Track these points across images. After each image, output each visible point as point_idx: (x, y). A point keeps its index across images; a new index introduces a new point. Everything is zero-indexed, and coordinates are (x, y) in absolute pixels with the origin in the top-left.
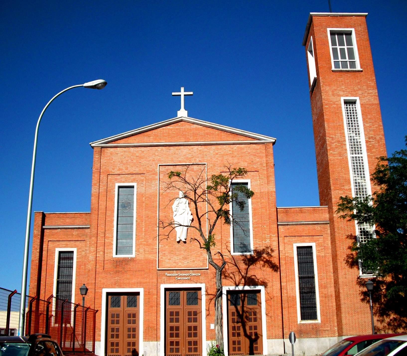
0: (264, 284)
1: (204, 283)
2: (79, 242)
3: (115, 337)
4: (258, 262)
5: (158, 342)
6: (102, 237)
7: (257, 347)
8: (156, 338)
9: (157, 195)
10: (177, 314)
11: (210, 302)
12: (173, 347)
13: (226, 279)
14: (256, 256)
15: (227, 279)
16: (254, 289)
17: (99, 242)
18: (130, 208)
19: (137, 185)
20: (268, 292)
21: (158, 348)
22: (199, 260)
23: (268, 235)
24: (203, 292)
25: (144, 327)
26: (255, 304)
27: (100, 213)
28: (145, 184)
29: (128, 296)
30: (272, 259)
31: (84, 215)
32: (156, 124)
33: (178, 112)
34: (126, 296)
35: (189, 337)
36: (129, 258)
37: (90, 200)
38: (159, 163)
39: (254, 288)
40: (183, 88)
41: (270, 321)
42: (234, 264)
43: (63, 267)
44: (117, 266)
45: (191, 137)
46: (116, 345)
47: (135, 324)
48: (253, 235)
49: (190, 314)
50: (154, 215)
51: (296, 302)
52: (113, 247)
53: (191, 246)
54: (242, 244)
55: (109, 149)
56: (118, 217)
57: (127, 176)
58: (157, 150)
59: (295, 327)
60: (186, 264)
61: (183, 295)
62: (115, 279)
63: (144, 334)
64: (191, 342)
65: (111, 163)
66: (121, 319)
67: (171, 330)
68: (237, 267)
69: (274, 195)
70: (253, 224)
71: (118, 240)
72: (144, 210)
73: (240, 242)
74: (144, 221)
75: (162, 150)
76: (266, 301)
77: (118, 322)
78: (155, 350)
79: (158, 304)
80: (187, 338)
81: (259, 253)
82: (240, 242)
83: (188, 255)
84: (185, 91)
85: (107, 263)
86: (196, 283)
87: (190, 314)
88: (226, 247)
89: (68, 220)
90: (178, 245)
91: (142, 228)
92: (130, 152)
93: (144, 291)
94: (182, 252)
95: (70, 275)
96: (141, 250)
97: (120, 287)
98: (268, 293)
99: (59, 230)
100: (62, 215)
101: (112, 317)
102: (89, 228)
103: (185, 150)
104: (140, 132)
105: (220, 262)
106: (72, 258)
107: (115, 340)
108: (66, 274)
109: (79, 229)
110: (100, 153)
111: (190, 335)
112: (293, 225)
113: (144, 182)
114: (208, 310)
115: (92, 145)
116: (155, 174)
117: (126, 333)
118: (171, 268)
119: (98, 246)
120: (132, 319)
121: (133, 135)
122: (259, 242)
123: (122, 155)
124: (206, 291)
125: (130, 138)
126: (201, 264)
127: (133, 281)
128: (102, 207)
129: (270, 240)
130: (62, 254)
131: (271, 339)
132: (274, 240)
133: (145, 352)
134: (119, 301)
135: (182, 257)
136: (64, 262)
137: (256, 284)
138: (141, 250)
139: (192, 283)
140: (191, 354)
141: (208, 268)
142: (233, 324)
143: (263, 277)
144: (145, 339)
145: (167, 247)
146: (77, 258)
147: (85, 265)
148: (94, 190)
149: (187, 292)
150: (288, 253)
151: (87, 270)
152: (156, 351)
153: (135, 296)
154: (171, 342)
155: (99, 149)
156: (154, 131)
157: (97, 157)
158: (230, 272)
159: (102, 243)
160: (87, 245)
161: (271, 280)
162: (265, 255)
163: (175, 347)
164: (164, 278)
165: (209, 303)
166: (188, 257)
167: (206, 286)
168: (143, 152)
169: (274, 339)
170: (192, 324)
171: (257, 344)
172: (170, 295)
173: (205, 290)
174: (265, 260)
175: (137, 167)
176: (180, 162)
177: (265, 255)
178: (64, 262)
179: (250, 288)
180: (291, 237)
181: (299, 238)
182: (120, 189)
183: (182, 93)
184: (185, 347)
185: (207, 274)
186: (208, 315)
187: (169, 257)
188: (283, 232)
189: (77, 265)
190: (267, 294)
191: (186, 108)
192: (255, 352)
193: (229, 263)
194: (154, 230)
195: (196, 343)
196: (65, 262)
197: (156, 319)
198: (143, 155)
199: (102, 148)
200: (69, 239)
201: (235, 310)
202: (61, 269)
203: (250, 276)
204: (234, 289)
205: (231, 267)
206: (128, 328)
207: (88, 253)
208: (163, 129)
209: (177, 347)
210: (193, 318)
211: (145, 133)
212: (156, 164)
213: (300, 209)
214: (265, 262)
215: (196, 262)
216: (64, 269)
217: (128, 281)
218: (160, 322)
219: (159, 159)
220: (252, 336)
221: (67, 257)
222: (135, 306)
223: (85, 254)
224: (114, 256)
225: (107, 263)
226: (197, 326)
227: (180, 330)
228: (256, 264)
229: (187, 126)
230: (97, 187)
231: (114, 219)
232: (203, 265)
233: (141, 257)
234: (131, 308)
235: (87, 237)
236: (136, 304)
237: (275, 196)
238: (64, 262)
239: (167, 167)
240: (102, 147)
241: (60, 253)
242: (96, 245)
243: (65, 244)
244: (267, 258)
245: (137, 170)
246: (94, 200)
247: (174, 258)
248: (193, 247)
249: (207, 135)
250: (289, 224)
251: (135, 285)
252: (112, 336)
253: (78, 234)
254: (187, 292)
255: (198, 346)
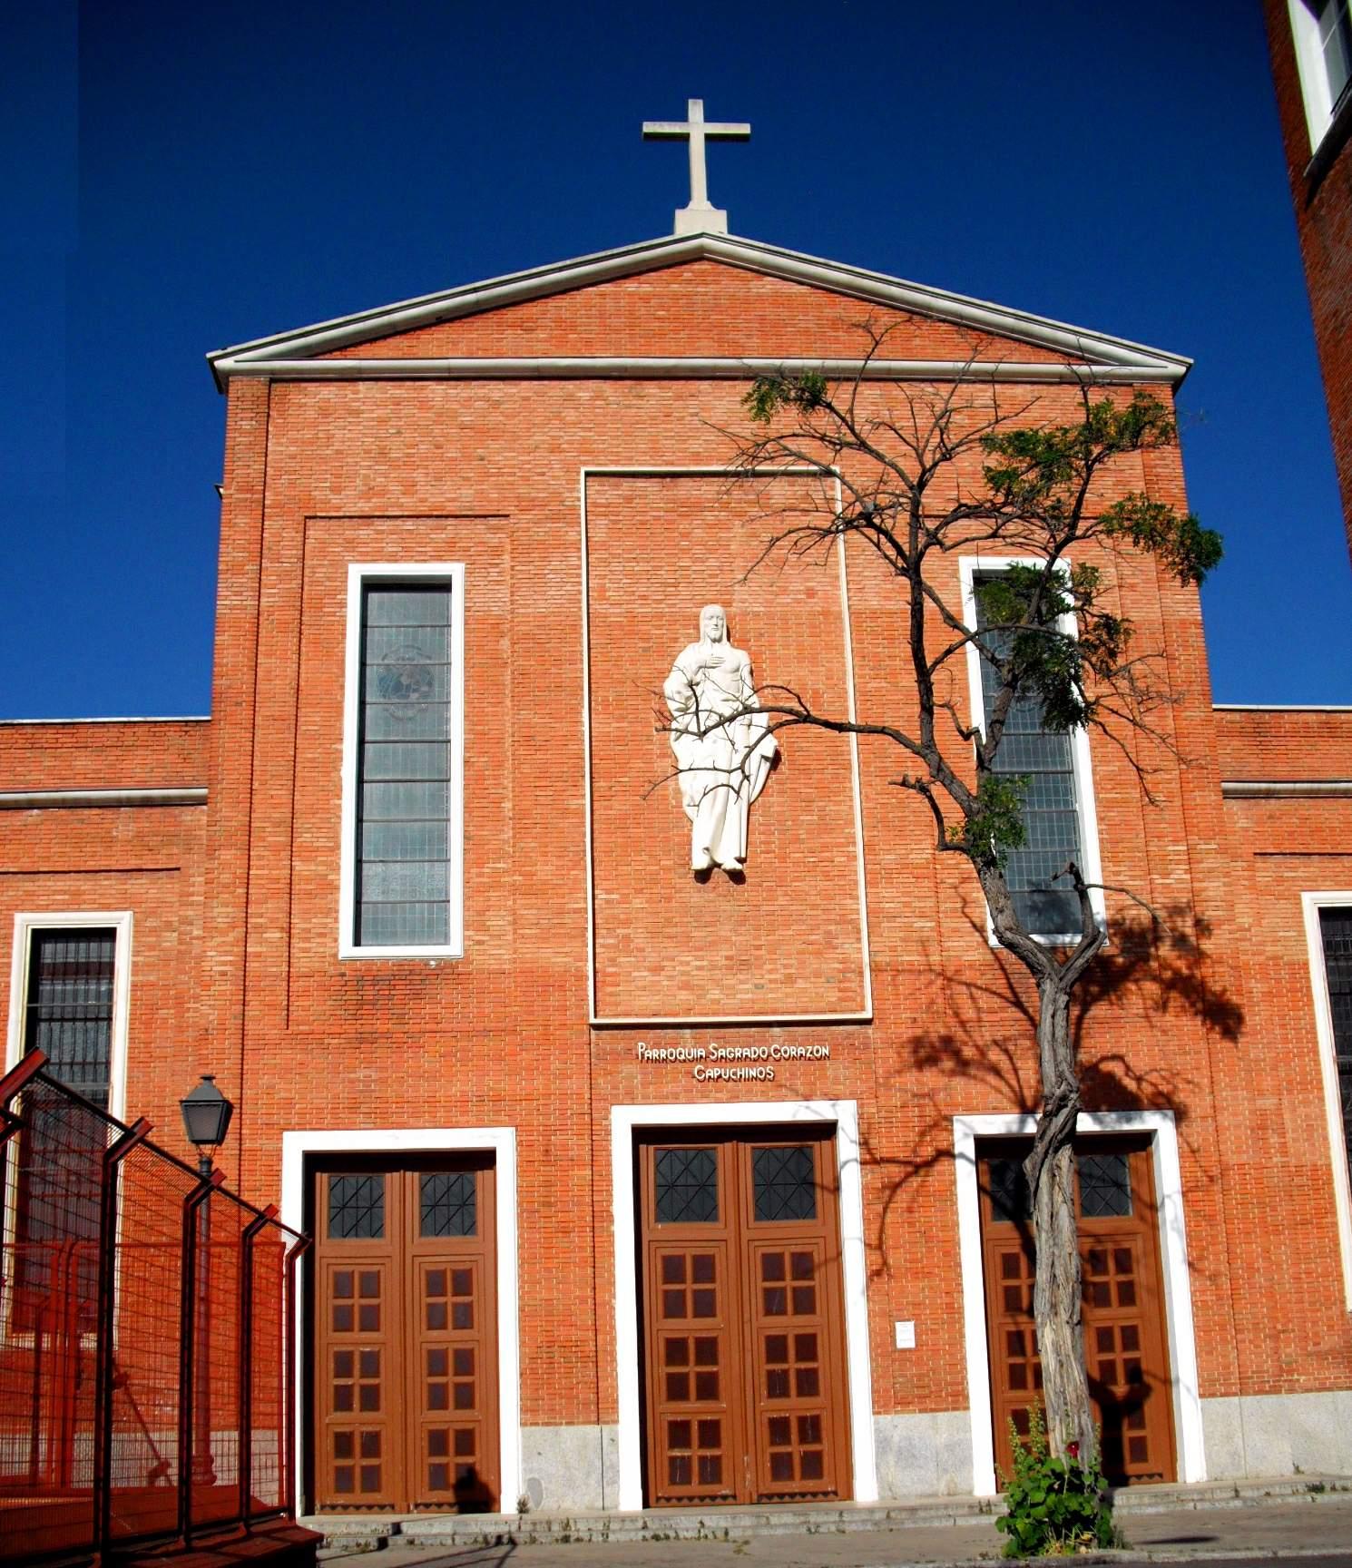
0: (1163, 1102)
1: (852, 1096)
2: (144, 880)
3: (356, 1405)
4: (1133, 987)
5: (606, 1428)
6: (276, 850)
7: (1142, 1440)
8: (593, 1407)
9: (576, 627)
10: (705, 1267)
11: (890, 1201)
12: (686, 1453)
13: (964, 1074)
14: (1123, 951)
15: (975, 1077)
16: (1126, 1127)
17: (259, 877)
18: (425, 695)
19: (468, 573)
20: (1195, 1146)
21: (607, 1463)
22: (817, 974)
23: (1175, 842)
24: (847, 1146)
25: (522, 1344)
26: (1121, 1210)
27: (266, 718)
28: (512, 568)
29: (426, 1177)
30: (1205, 971)
31: (172, 733)
32: (568, 262)
33: (679, 214)
34: (416, 1175)
35: (771, 1395)
36: (427, 965)
37: (208, 650)
38: (585, 463)
39: (1119, 1121)
40: (701, 102)
41: (1209, 1297)
42: (1008, 994)
43: (57, 1016)
44: (361, 1004)
45: (749, 336)
46: (363, 1445)
47: (472, 1327)
48: (1101, 841)
49: (772, 1266)
50: (563, 728)
51: (1332, 1196)
52: (337, 902)
53: (772, 899)
54: (1040, 891)
55: (311, 387)
56: (361, 742)
57: (409, 525)
58: (570, 397)
59: (1331, 1327)
60: (750, 996)
61: (734, 1164)
62: (352, 1081)
63: (523, 1386)
64: (786, 1421)
65: (324, 460)
66: (388, 1301)
67: (671, 1360)
68: (1025, 1012)
69: (1196, 637)
70: (1098, 786)
71: (365, 865)
72: (508, 703)
73: (1030, 882)
74: (509, 764)
75: (597, 398)
76: (1184, 1194)
77: (371, 1321)
78: (588, 1474)
79: (600, 1217)
80: (764, 1403)
81: (1138, 941)
82: (1030, 882)
83: (758, 948)
84: (709, 118)
85: (306, 993)
86: (807, 1098)
87: (772, 1266)
88: (959, 905)
89: (83, 762)
90: (697, 895)
91: (498, 803)
92: (424, 405)
93: (520, 1144)
94: (725, 931)
95: (95, 1064)
96: (498, 921)
97: (383, 1121)
98: (1193, 1151)
99: (35, 812)
100: (50, 734)
101: (338, 1294)
102: (201, 801)
103: (721, 398)
104: (477, 303)
105: (931, 983)
106: (106, 970)
107: (356, 1420)
108: (85, 1056)
109: (147, 811)
110: (264, 408)
111: (777, 1386)
112: (1293, 794)
113: (507, 557)
114: (876, 1245)
115: (218, 364)
116: (569, 516)
117: (420, 1380)
118: (666, 1015)
119: (252, 898)
120: (450, 1299)
121: (440, 320)
122: (1133, 878)
123: (382, 421)
124: (864, 1144)
125: (424, 336)
126: (833, 996)
127: (455, 1090)
128: (276, 685)
129: (1186, 872)
130: (48, 948)
131: (1222, 1395)
132: (1211, 871)
133: (533, 1484)
134: (375, 1204)
135: (727, 958)
136: (64, 992)
137: (1129, 1103)
138: (498, 921)
139: (782, 1099)
140: (786, 1491)
141: (868, 1015)
142: (1009, 1320)
143: (1162, 1064)
144: (534, 1411)
145: (638, 903)
146: (135, 964)
147: (180, 1002)
148: (231, 599)
149: (753, 1148)
150: (1276, 941)
151: (191, 1034)
152: (594, 1479)
153: (468, 1175)
154: (674, 1426)
155: (259, 388)
156: (552, 303)
157: (246, 425)
158: (988, 1037)
159: (277, 880)
160: (192, 894)
161: (1206, 1081)
162: (1165, 950)
163: (695, 1452)
164: (629, 1068)
165: (880, 1208)
166: (758, 958)
167: (861, 1116)
168: (496, 404)
169: (1235, 1394)
170: (790, 1324)
171: (1140, 1424)
172: (662, 1167)
173: (855, 1135)
174: (1168, 974)
175: (467, 479)
176: (697, 458)
177: (1165, 950)
178: (64, 992)
179: (1099, 1121)
180: (1289, 859)
181: (1328, 863)
182: (374, 597)
183: (697, 126)
184: (751, 1448)
185: (866, 1046)
186: (875, 1274)
187: (652, 958)
188: (1246, 830)
189: (135, 1001)
190: (1189, 1153)
191: (716, 198)
192: (1131, 1468)
193: (979, 988)
194: (565, 812)
195: (811, 1429)
196: (69, 987)
197: (590, 1301)
198: (495, 418)
199: (272, 381)
200: (91, 865)
201: (1018, 1241)
202: (43, 1026)
203: (1094, 1060)
204: (1015, 1128)
205: (991, 1011)
206: (430, 1352)
207: (197, 938)
208: (603, 295)
209: (709, 1453)
210: (795, 1290)
211: (504, 311)
212: (571, 470)
213: (1324, 716)
214: (1169, 986)
215: (801, 984)
216: (62, 1032)
217: (424, 1089)
218: (612, 1317)
219: (584, 440)
220: (1114, 1382)
221: (65, 964)
222: (470, 1229)
223: (181, 942)
224: (346, 949)
225: (306, 993)
226: (813, 1337)
227: (721, 1360)
228: (1119, 998)
229: (730, 285)
230: (246, 581)
231: (341, 752)
232: (841, 1000)
233: (499, 955)
234: (443, 1239)
235: (189, 850)
236: (381, 1219)
237: (1200, 642)
238: (59, 988)
239: (627, 484)
240: (276, 378)
241: (40, 937)
242: (242, 891)
243: (65, 893)
244: (1181, 965)
245: (465, 497)
246: (229, 650)
247: (681, 963)
248: (782, 901)
249: (836, 330)
250: (1279, 792)
251: (465, 1113)
252: (343, 1399)
253: (140, 835)
254: (753, 1148)
255: (825, 1446)
